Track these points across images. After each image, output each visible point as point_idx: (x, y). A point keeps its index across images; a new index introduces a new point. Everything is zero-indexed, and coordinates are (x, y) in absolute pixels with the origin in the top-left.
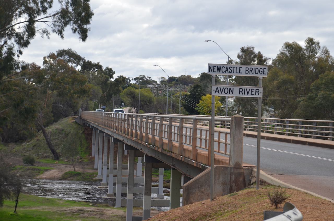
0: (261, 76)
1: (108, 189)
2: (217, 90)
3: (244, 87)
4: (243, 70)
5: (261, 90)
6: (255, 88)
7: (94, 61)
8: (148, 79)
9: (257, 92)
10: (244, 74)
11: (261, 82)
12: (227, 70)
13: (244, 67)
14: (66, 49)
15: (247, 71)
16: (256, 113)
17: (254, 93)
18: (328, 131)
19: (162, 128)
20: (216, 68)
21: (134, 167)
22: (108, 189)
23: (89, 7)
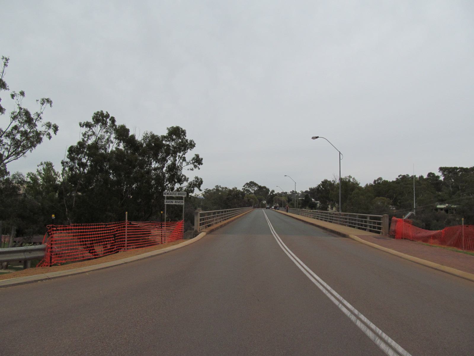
0: (184, 196)
1: (200, 217)
2: (167, 202)
3: (177, 201)
4: (177, 194)
5: (184, 201)
6: (181, 201)
7: (262, 186)
8: (401, 177)
9: (182, 202)
10: (177, 196)
11: (184, 199)
12: (171, 194)
13: (177, 193)
14: (433, 172)
15: (178, 194)
16: (265, 202)
17: (181, 203)
18: (355, 218)
19: (128, 214)
20: (167, 193)
21: (10, 238)
22: (200, 217)
23: (470, 168)
